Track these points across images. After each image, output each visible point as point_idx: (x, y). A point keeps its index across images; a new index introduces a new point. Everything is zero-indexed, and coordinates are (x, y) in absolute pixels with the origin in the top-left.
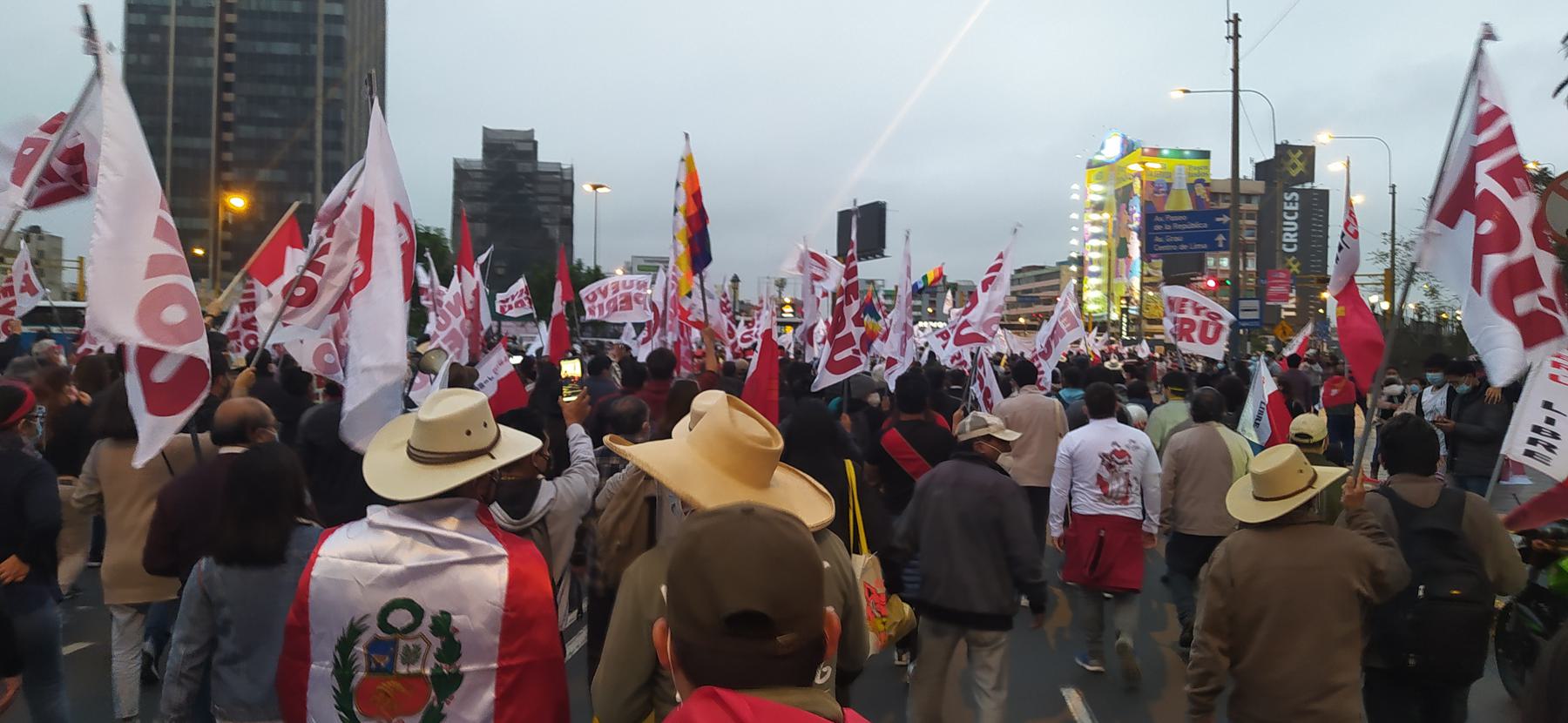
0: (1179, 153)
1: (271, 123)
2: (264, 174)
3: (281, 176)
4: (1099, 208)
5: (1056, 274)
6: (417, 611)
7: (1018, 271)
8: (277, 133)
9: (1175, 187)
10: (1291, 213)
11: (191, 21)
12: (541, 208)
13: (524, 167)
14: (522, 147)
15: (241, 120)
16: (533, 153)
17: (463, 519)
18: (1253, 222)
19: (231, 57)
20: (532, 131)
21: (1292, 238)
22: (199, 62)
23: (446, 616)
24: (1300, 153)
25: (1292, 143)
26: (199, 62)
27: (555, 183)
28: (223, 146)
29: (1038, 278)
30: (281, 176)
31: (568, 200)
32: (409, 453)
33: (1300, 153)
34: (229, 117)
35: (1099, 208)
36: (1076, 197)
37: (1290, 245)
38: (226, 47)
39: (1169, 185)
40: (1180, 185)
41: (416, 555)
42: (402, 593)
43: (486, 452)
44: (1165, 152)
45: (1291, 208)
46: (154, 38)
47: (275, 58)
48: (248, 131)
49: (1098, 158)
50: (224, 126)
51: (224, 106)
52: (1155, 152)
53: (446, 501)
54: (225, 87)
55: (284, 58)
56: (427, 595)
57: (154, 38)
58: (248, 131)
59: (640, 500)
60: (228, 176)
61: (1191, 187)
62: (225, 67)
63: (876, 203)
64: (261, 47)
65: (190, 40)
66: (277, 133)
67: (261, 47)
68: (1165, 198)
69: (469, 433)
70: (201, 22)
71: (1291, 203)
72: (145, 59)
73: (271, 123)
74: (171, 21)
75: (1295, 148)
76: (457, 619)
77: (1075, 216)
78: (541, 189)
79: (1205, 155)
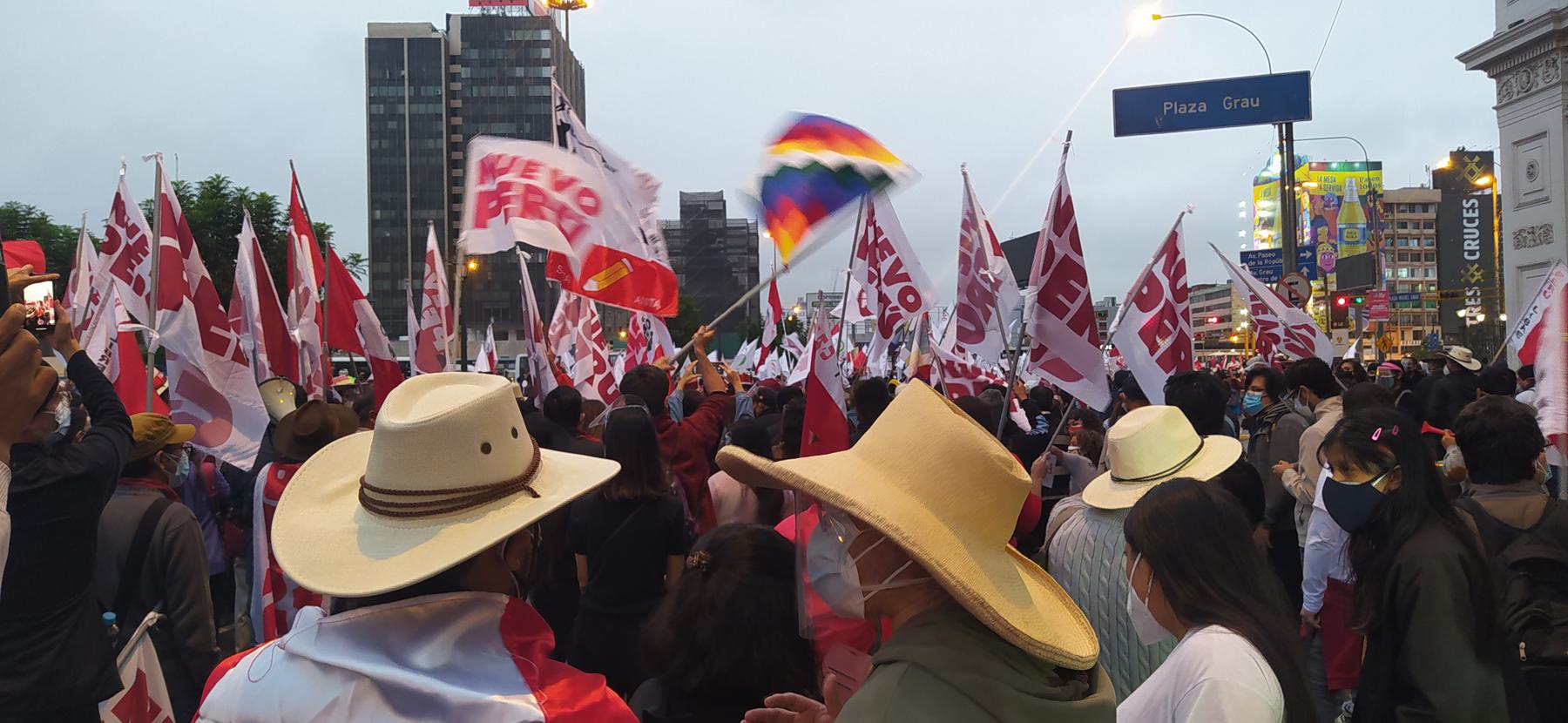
0: (1349, 166)
4: (1268, 224)
9: (1347, 199)
10: (1471, 220)
11: (422, 109)
12: (731, 259)
13: (714, 223)
14: (711, 207)
16: (721, 213)
17: (469, 642)
18: (1432, 231)
21: (1474, 246)
22: (431, 144)
24: (1477, 159)
25: (1468, 149)
26: (431, 144)
27: (742, 236)
29: (1208, 297)
31: (754, 251)
32: (363, 499)
33: (1477, 159)
35: (1268, 224)
36: (1243, 214)
37: (1472, 253)
39: (1340, 198)
40: (1352, 196)
43: (521, 484)
44: (1334, 166)
45: (1470, 214)
46: (392, 125)
49: (1266, 174)
52: (1324, 166)
53: (414, 607)
57: (392, 125)
61: (1363, 199)
68: (1336, 213)
69: (486, 448)
70: (431, 109)
71: (1470, 210)
72: (385, 144)
74: (406, 109)
75: (1472, 155)
77: (1242, 234)
78: (729, 242)
79: (1377, 166)
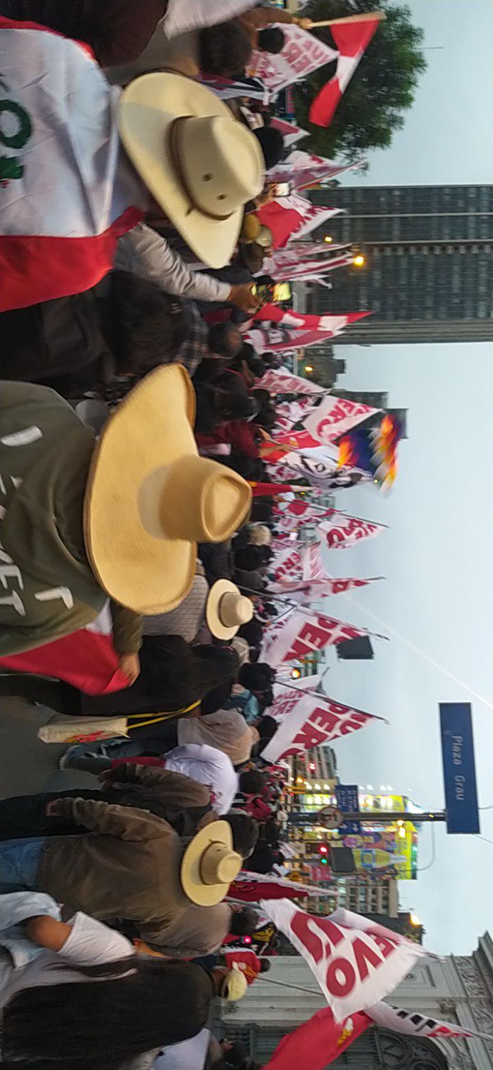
0: (414, 859)
1: (409, 277)
2: (377, 274)
3: (377, 284)
5: (331, 776)
6: (19, 141)
7: (332, 751)
8: (403, 281)
9: (392, 856)
11: (472, 225)
15: (410, 257)
19: (450, 251)
20: (406, 438)
23: (19, 172)
28: (394, 248)
29: (328, 764)
30: (377, 284)
34: (413, 251)
35: (376, 804)
38: (456, 247)
39: (392, 852)
40: (394, 859)
41: (85, 140)
42: (38, 124)
46: (461, 203)
47: (449, 277)
48: (404, 263)
50: (407, 248)
51: (419, 247)
54: (431, 247)
55: (450, 283)
56: (40, 153)
58: (404, 263)
59: (229, 721)
60: (376, 253)
61: (392, 866)
62: (444, 247)
63: (372, 653)
64: (456, 268)
65: (459, 226)
66: (403, 281)
67: (456, 268)
69: (207, 178)
73: (409, 277)
76: (16, 184)
79: (414, 877)
